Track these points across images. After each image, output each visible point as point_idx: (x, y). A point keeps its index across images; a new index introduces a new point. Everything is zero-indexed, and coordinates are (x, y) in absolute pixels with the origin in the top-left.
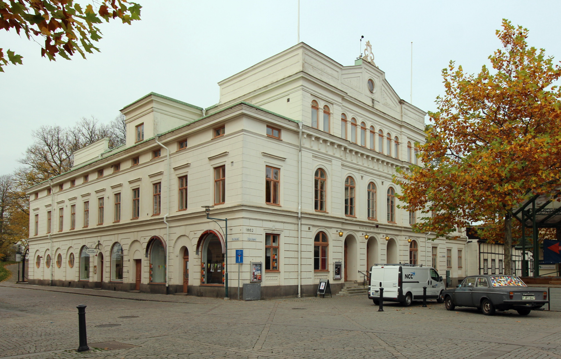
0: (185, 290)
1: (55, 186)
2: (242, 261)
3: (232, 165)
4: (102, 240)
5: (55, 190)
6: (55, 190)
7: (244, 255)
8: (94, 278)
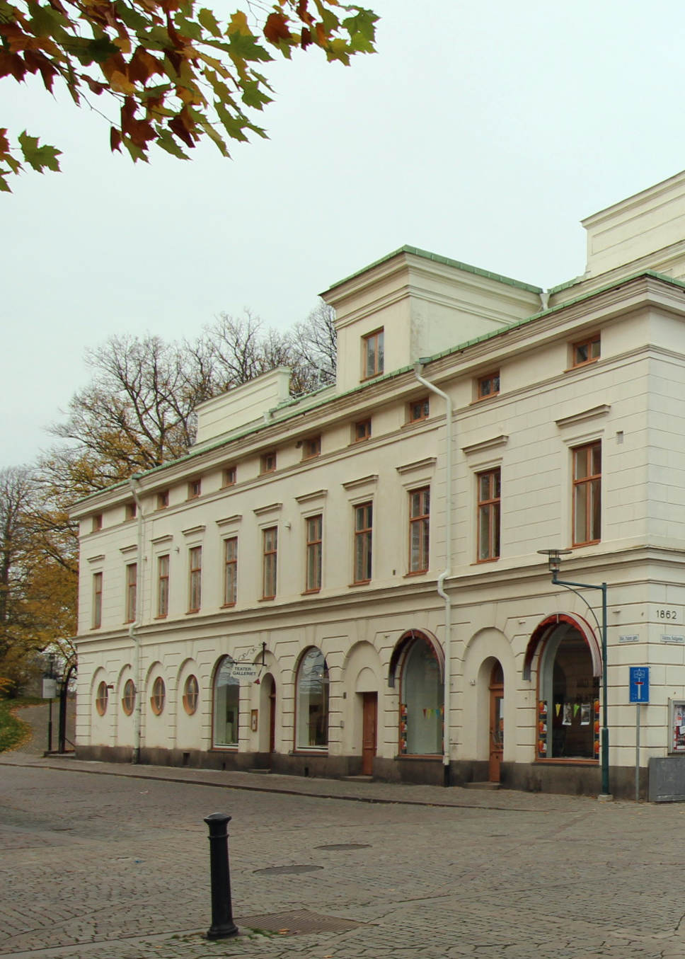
0: (495, 774)
1: (146, 495)
2: (645, 696)
3: (620, 441)
4: (273, 640)
5: (148, 507)
6: (148, 507)
7: (651, 681)
8: (250, 742)
